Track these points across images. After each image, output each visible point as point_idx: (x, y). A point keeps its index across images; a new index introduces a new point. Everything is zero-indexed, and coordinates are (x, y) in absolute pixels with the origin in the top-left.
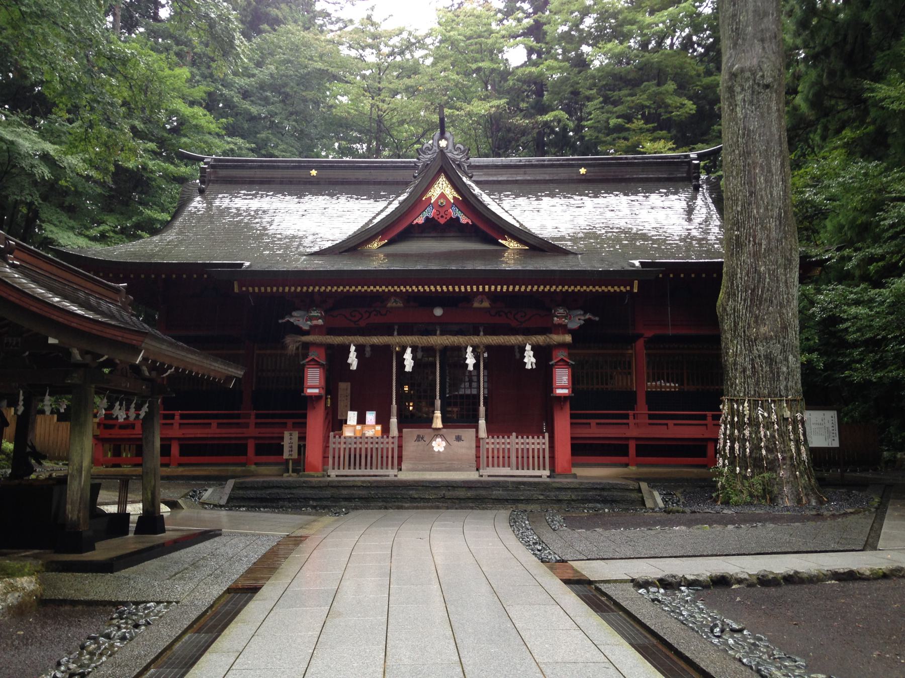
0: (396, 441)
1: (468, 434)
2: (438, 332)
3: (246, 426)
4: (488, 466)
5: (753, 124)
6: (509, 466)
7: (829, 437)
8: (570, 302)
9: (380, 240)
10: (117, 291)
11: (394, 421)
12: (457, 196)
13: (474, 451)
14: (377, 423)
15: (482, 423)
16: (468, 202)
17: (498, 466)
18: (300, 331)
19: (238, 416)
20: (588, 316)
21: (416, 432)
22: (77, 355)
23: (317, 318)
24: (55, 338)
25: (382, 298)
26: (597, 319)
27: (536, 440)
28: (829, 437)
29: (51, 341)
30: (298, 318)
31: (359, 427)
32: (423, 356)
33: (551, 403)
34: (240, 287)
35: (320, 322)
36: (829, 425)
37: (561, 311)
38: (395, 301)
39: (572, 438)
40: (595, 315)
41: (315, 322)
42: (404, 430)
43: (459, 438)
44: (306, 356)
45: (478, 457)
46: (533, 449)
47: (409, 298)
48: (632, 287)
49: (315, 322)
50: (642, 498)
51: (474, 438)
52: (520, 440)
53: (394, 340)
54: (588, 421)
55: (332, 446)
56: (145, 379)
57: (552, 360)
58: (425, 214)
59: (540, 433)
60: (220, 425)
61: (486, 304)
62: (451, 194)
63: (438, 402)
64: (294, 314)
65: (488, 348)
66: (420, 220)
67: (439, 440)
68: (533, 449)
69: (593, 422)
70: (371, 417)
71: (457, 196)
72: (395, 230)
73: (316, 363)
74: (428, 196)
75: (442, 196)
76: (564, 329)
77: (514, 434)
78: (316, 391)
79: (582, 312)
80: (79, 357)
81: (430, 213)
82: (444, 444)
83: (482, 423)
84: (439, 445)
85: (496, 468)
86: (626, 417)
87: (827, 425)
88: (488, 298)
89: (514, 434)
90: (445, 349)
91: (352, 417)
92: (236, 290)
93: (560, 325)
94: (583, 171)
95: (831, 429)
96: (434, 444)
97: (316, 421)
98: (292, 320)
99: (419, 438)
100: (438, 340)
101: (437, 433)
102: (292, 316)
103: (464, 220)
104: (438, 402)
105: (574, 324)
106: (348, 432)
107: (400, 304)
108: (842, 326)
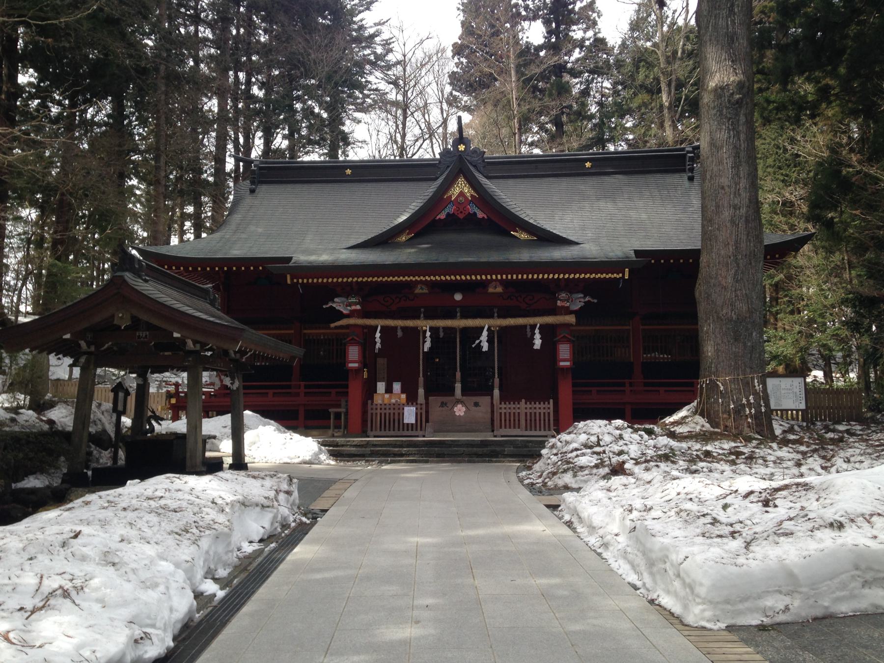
0: (424, 407)
1: (485, 400)
2: (458, 314)
3: (298, 394)
4: (501, 427)
6: (519, 427)
7: (797, 400)
8: (572, 287)
9: (408, 234)
10: (206, 291)
11: (421, 391)
13: (489, 416)
14: (402, 392)
15: (496, 392)
16: (484, 199)
17: (510, 427)
18: (340, 315)
19: (289, 387)
20: (587, 299)
21: (441, 399)
22: (190, 344)
23: (356, 304)
25: (410, 285)
26: (596, 301)
27: (542, 405)
28: (797, 400)
29: (176, 335)
30: (339, 304)
31: (387, 396)
33: (555, 372)
34: (292, 279)
35: (358, 307)
36: (797, 390)
37: (564, 295)
38: (422, 288)
39: (574, 404)
40: (593, 298)
41: (353, 307)
42: (430, 398)
43: (476, 404)
45: (492, 420)
46: (540, 413)
47: (432, 285)
48: (624, 275)
49: (353, 307)
51: (489, 404)
52: (529, 406)
54: (590, 389)
55: (370, 412)
56: (232, 360)
58: (447, 210)
59: (544, 399)
61: (499, 289)
62: (468, 191)
63: (458, 375)
64: (336, 300)
66: (442, 216)
67: (460, 406)
68: (540, 413)
69: (662, 389)
70: (397, 387)
72: (422, 226)
75: (462, 194)
76: (567, 311)
77: (523, 401)
79: (582, 295)
80: (192, 346)
81: (450, 209)
82: (464, 409)
83: (496, 392)
84: (460, 410)
85: (512, 429)
86: (623, 385)
87: (795, 390)
88: (501, 284)
89: (523, 401)
90: (465, 330)
91: (381, 387)
92: (289, 282)
93: (563, 307)
96: (455, 409)
97: (355, 390)
98: (334, 305)
99: (443, 404)
101: (459, 401)
102: (334, 302)
103: (480, 215)
104: (458, 375)
105: (577, 306)
106: (378, 400)
107: (425, 291)
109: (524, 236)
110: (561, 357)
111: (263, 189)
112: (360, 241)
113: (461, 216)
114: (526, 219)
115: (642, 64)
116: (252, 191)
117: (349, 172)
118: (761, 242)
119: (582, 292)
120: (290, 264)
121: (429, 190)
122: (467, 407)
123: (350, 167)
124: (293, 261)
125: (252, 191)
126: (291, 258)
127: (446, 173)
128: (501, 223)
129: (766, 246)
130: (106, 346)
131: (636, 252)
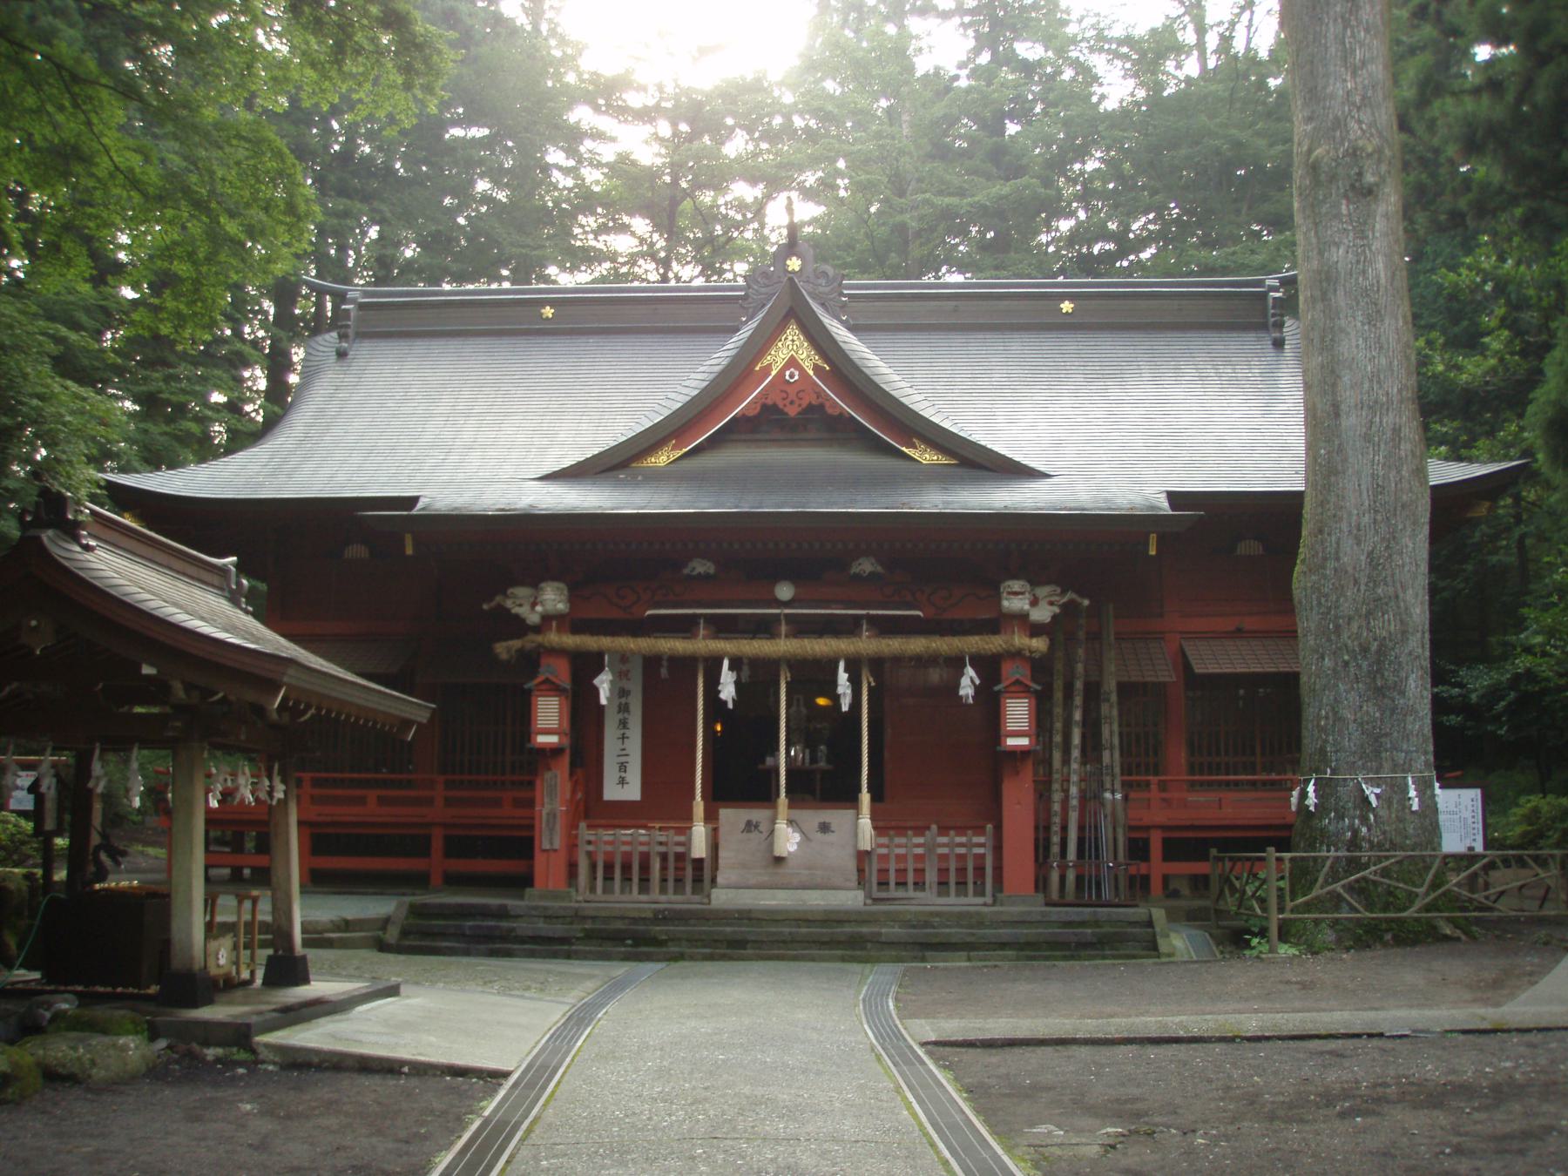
5: (1366, 252)
10: (223, 571)
12: (820, 363)
16: (841, 370)
24: (152, 665)
29: (147, 670)
32: (757, 677)
36: (1468, 814)
43: (825, 828)
44: (533, 673)
46: (593, 889)
50: (1154, 935)
53: (702, 644)
57: (999, 682)
60: (382, 801)
62: (808, 358)
65: (877, 664)
71: (820, 363)
72: (712, 426)
73: (553, 688)
74: (766, 363)
78: (554, 739)
94: (1067, 306)
95: (1470, 820)
99: (750, 826)
100: (783, 646)
108: (217, 1013)
109: (926, 457)
110: (1011, 727)
111: (362, 351)
112: (567, 462)
113: (792, 411)
114: (935, 419)
115: (663, 254)
116: (342, 355)
117: (548, 312)
118: (1426, 477)
119: (1056, 583)
120: (414, 512)
121: (718, 356)
122: (802, 833)
123: (551, 303)
124: (420, 505)
125: (342, 355)
126: (415, 500)
127: (760, 316)
128: (874, 425)
129: (1434, 488)
130: (8, 689)
131: (1172, 496)
